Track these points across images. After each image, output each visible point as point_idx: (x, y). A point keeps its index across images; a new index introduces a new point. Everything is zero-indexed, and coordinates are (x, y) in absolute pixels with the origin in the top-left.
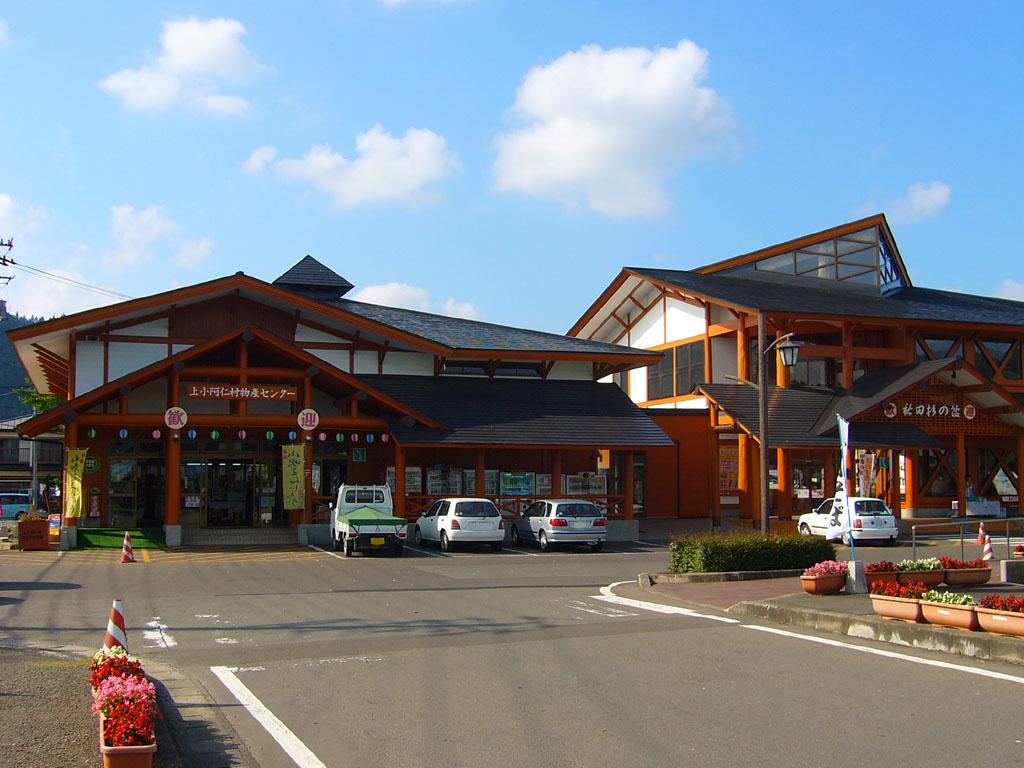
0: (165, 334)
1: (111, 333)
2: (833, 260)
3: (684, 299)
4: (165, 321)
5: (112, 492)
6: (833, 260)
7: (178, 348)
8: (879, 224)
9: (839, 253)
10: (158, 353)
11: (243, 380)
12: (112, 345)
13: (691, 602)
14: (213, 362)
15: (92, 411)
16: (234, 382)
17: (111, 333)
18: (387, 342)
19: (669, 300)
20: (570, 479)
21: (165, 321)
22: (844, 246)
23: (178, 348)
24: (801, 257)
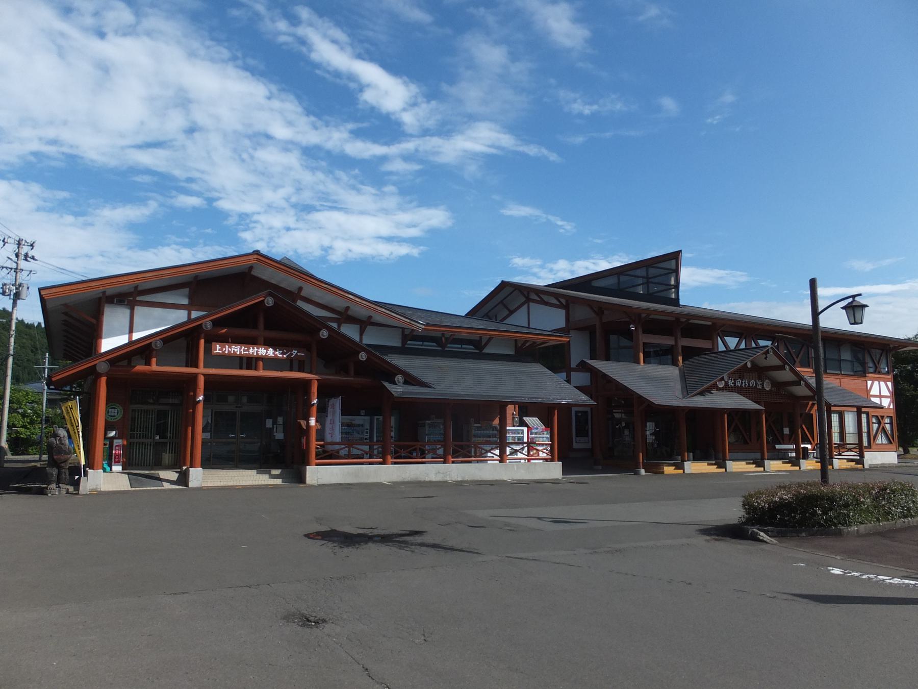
0: (185, 301)
1: (138, 298)
2: (645, 280)
3: (547, 304)
4: (186, 291)
5: (158, 437)
6: (645, 280)
7: (195, 314)
8: (40, 290)
9: (650, 276)
10: (178, 317)
11: (261, 340)
12: (138, 310)
13: (739, 273)
14: (242, 326)
15: (120, 364)
16: (253, 342)
17: (138, 298)
18: (370, 317)
19: (531, 304)
20: (586, 412)
21: (186, 291)
22: (652, 271)
23: (195, 314)
24: (623, 278)
